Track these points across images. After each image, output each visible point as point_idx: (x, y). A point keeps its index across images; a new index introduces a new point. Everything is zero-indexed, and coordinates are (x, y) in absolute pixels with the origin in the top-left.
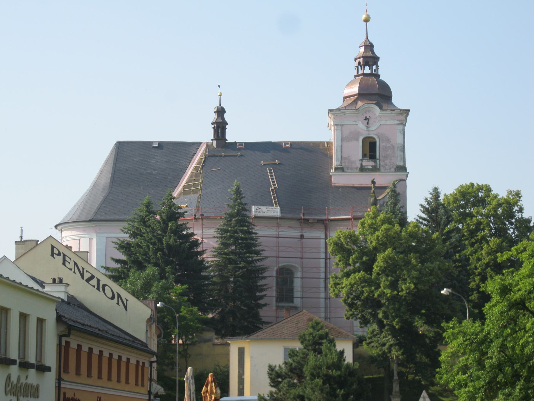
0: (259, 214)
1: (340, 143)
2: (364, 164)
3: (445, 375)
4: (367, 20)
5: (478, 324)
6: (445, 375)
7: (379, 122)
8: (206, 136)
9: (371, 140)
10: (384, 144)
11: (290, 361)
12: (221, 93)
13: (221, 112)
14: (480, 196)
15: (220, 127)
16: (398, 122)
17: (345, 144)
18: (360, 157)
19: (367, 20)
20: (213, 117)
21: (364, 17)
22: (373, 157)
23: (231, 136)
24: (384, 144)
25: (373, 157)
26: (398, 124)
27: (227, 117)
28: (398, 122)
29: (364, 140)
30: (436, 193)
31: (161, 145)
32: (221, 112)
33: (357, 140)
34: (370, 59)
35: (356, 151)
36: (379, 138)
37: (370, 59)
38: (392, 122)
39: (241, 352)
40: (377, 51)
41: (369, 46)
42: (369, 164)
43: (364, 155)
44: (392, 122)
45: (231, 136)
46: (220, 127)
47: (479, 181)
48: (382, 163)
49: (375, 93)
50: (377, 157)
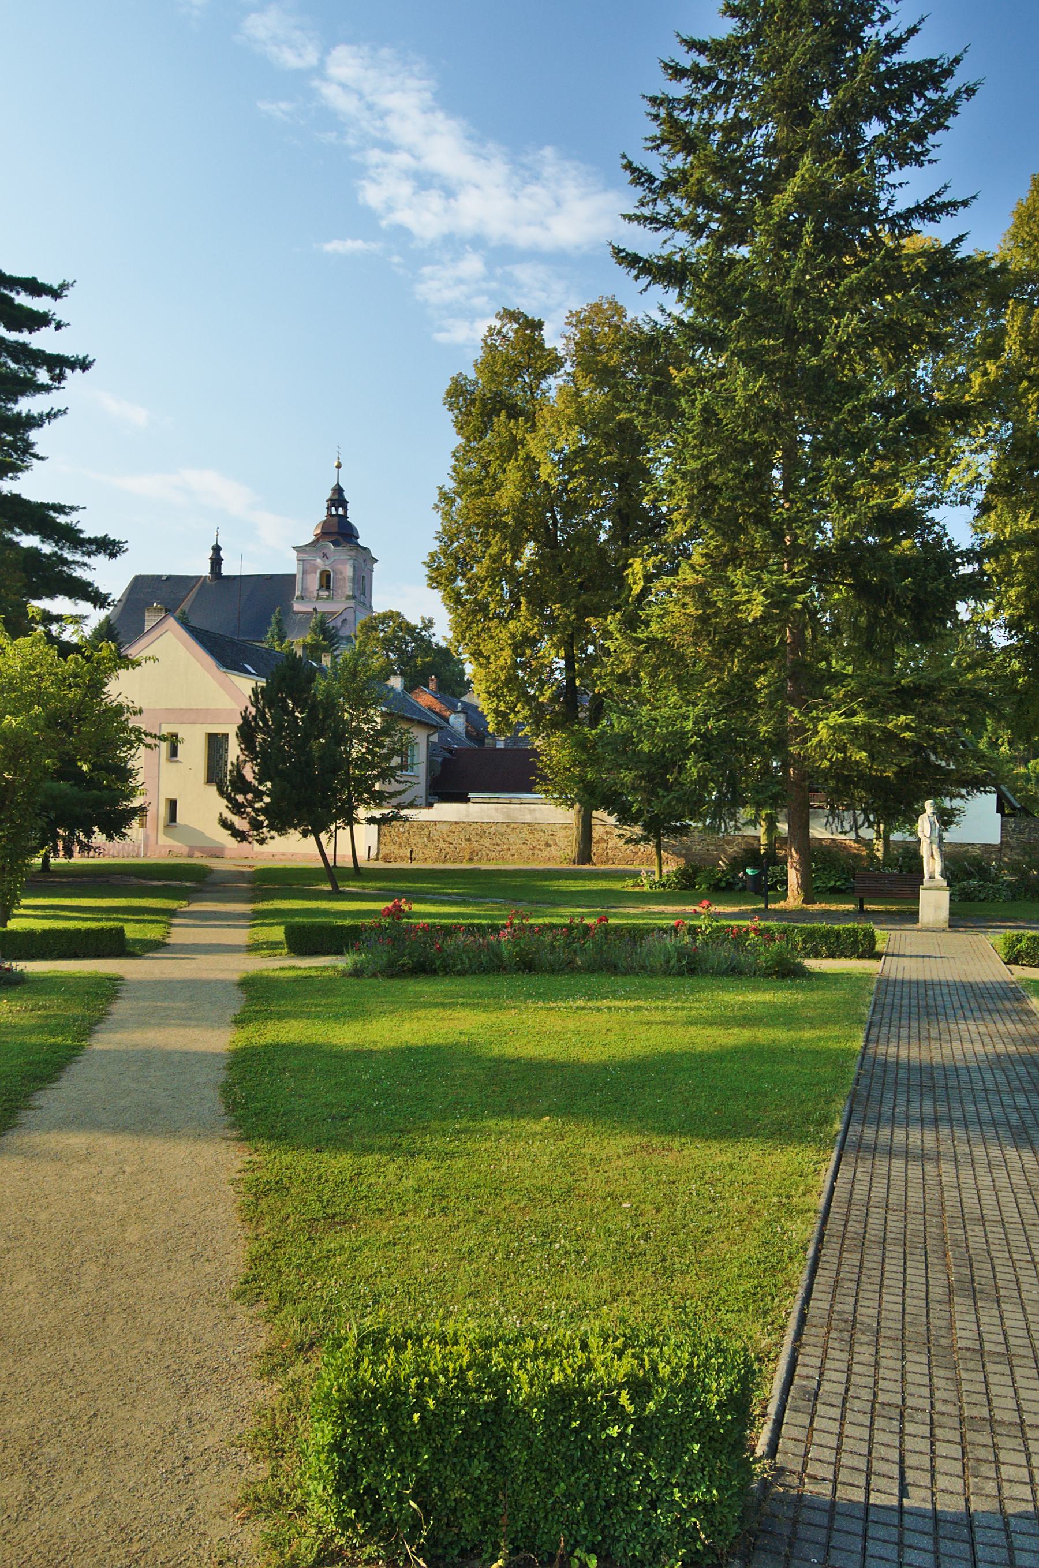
0: (878, 1502)
4: (339, 467)
11: (896, 167)
13: (217, 549)
15: (216, 561)
19: (339, 467)
22: (328, 588)
23: (225, 571)
25: (328, 588)
27: (222, 554)
29: (322, 573)
31: (169, 578)
32: (217, 549)
34: (338, 499)
35: (314, 582)
37: (338, 499)
40: (347, 495)
41: (338, 490)
42: (324, 594)
43: (321, 587)
45: (225, 571)
46: (216, 561)
47: (1013, 207)
49: (339, 531)
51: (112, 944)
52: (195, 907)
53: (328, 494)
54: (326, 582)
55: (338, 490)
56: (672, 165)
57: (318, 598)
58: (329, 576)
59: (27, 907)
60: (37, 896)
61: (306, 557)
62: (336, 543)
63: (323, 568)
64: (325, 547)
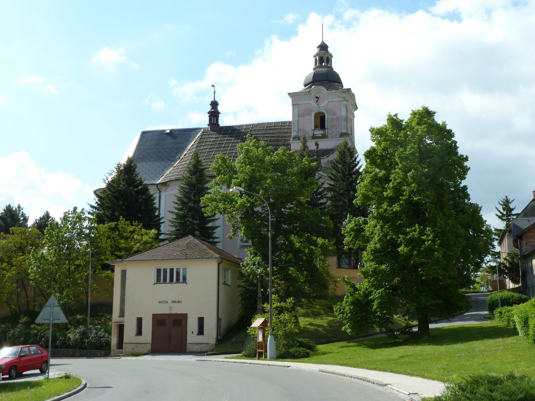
7: (328, 100)
8: (201, 121)
9: (322, 114)
13: (214, 104)
15: (214, 114)
16: (341, 99)
20: (209, 108)
23: (224, 121)
27: (220, 108)
28: (341, 99)
29: (316, 115)
32: (214, 104)
33: (310, 115)
38: (337, 99)
39: (124, 273)
41: (323, 47)
42: (319, 133)
43: (316, 127)
44: (337, 99)
45: (224, 121)
46: (214, 114)
48: (330, 132)
50: (326, 127)
53: (316, 51)
63: (316, 110)
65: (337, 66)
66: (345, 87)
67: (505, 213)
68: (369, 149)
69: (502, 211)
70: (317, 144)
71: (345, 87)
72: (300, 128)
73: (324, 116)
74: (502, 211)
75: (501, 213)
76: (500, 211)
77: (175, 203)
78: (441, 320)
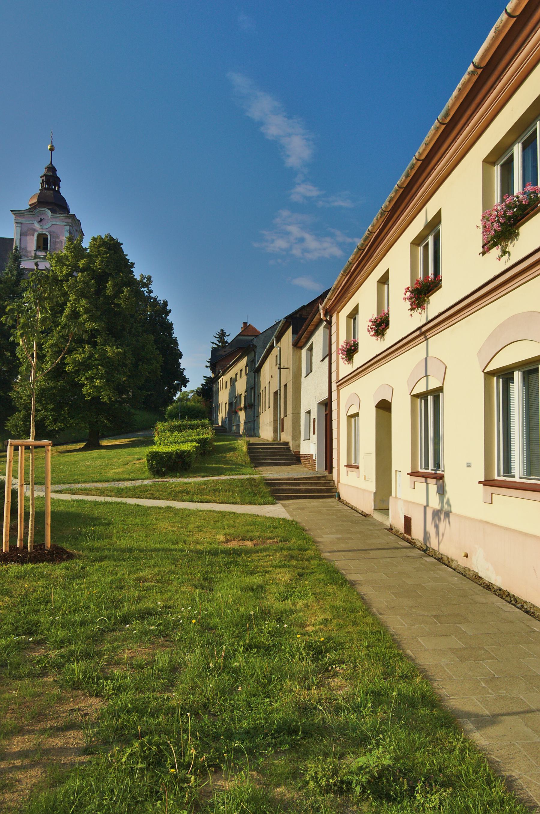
1: (19, 237)
2: (38, 253)
3: (153, 337)
4: (52, 150)
5: (106, 581)
6: (153, 337)
9: (45, 236)
10: (54, 240)
12: (52, 146)
14: (110, 354)
16: (66, 224)
17: (23, 237)
18: (34, 248)
21: (49, 147)
22: (45, 249)
24: (54, 240)
26: (66, 225)
28: (66, 224)
29: (39, 236)
30: (122, 244)
33: (33, 235)
34: (51, 179)
35: (32, 244)
36: (50, 235)
37: (51, 179)
38: (62, 223)
39: (427, 465)
41: (52, 169)
42: (41, 254)
43: (38, 248)
44: (62, 223)
50: (49, 249)
51: (27, 514)
52: (378, 230)
53: (43, 172)
54: (43, 243)
55: (52, 169)
56: (367, 805)
57: (36, 257)
58: (46, 240)
59: (27, 460)
60: (494, 187)
61: (20, 219)
62: (53, 211)
63: (40, 231)
64: (43, 213)
65: (65, 190)
66: (71, 212)
67: (220, 344)
68: (387, 330)
69: (217, 343)
70: (37, 264)
71: (71, 212)
72: (22, 246)
73: (48, 239)
74: (217, 343)
75: (217, 345)
76: (216, 344)
77: (213, 343)
78: (123, 433)
